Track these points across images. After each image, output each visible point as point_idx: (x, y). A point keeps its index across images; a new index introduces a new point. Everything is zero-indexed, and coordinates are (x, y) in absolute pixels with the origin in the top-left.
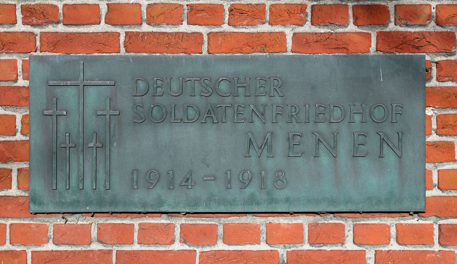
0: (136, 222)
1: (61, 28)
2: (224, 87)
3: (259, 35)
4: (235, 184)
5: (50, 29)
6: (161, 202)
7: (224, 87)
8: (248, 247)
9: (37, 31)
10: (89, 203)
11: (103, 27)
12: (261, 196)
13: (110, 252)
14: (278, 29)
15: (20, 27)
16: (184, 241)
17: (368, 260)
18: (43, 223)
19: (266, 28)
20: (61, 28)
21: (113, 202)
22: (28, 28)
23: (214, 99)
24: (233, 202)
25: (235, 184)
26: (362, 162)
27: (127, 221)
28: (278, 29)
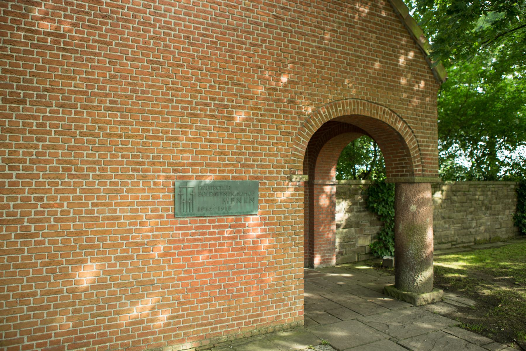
0: (198, 219)
1: (181, 174)
2: (218, 188)
3: (225, 176)
4: (220, 210)
5: (178, 174)
6: (204, 214)
7: (218, 188)
8: (222, 224)
9: (176, 174)
10: (188, 215)
11: (190, 174)
12: (226, 212)
13: (45, 211)
14: (228, 174)
15: (171, 174)
16: (209, 223)
17: (503, 234)
18: (221, 325)
19: (226, 174)
20: (181, 174)
21: (194, 214)
22: (173, 174)
23: (216, 191)
24: (220, 214)
25: (220, 210)
26: (246, 204)
27: (196, 219)
28: (228, 174)
